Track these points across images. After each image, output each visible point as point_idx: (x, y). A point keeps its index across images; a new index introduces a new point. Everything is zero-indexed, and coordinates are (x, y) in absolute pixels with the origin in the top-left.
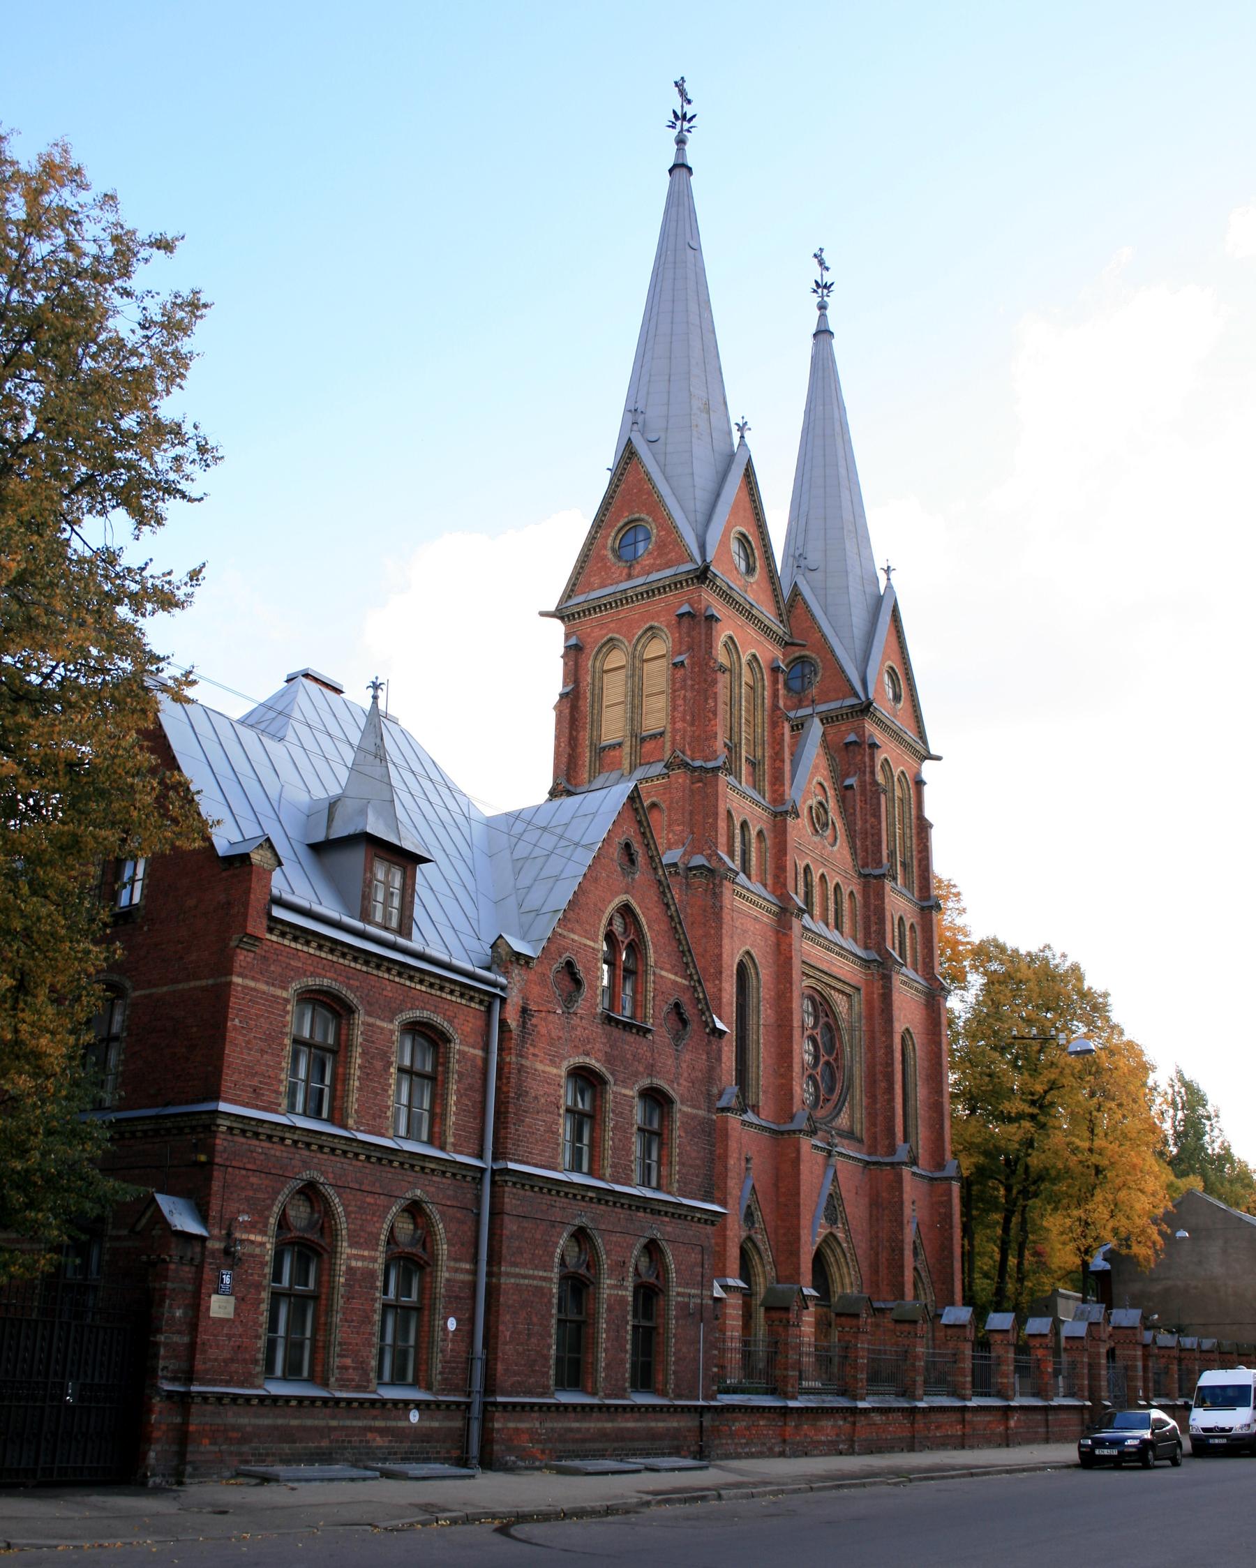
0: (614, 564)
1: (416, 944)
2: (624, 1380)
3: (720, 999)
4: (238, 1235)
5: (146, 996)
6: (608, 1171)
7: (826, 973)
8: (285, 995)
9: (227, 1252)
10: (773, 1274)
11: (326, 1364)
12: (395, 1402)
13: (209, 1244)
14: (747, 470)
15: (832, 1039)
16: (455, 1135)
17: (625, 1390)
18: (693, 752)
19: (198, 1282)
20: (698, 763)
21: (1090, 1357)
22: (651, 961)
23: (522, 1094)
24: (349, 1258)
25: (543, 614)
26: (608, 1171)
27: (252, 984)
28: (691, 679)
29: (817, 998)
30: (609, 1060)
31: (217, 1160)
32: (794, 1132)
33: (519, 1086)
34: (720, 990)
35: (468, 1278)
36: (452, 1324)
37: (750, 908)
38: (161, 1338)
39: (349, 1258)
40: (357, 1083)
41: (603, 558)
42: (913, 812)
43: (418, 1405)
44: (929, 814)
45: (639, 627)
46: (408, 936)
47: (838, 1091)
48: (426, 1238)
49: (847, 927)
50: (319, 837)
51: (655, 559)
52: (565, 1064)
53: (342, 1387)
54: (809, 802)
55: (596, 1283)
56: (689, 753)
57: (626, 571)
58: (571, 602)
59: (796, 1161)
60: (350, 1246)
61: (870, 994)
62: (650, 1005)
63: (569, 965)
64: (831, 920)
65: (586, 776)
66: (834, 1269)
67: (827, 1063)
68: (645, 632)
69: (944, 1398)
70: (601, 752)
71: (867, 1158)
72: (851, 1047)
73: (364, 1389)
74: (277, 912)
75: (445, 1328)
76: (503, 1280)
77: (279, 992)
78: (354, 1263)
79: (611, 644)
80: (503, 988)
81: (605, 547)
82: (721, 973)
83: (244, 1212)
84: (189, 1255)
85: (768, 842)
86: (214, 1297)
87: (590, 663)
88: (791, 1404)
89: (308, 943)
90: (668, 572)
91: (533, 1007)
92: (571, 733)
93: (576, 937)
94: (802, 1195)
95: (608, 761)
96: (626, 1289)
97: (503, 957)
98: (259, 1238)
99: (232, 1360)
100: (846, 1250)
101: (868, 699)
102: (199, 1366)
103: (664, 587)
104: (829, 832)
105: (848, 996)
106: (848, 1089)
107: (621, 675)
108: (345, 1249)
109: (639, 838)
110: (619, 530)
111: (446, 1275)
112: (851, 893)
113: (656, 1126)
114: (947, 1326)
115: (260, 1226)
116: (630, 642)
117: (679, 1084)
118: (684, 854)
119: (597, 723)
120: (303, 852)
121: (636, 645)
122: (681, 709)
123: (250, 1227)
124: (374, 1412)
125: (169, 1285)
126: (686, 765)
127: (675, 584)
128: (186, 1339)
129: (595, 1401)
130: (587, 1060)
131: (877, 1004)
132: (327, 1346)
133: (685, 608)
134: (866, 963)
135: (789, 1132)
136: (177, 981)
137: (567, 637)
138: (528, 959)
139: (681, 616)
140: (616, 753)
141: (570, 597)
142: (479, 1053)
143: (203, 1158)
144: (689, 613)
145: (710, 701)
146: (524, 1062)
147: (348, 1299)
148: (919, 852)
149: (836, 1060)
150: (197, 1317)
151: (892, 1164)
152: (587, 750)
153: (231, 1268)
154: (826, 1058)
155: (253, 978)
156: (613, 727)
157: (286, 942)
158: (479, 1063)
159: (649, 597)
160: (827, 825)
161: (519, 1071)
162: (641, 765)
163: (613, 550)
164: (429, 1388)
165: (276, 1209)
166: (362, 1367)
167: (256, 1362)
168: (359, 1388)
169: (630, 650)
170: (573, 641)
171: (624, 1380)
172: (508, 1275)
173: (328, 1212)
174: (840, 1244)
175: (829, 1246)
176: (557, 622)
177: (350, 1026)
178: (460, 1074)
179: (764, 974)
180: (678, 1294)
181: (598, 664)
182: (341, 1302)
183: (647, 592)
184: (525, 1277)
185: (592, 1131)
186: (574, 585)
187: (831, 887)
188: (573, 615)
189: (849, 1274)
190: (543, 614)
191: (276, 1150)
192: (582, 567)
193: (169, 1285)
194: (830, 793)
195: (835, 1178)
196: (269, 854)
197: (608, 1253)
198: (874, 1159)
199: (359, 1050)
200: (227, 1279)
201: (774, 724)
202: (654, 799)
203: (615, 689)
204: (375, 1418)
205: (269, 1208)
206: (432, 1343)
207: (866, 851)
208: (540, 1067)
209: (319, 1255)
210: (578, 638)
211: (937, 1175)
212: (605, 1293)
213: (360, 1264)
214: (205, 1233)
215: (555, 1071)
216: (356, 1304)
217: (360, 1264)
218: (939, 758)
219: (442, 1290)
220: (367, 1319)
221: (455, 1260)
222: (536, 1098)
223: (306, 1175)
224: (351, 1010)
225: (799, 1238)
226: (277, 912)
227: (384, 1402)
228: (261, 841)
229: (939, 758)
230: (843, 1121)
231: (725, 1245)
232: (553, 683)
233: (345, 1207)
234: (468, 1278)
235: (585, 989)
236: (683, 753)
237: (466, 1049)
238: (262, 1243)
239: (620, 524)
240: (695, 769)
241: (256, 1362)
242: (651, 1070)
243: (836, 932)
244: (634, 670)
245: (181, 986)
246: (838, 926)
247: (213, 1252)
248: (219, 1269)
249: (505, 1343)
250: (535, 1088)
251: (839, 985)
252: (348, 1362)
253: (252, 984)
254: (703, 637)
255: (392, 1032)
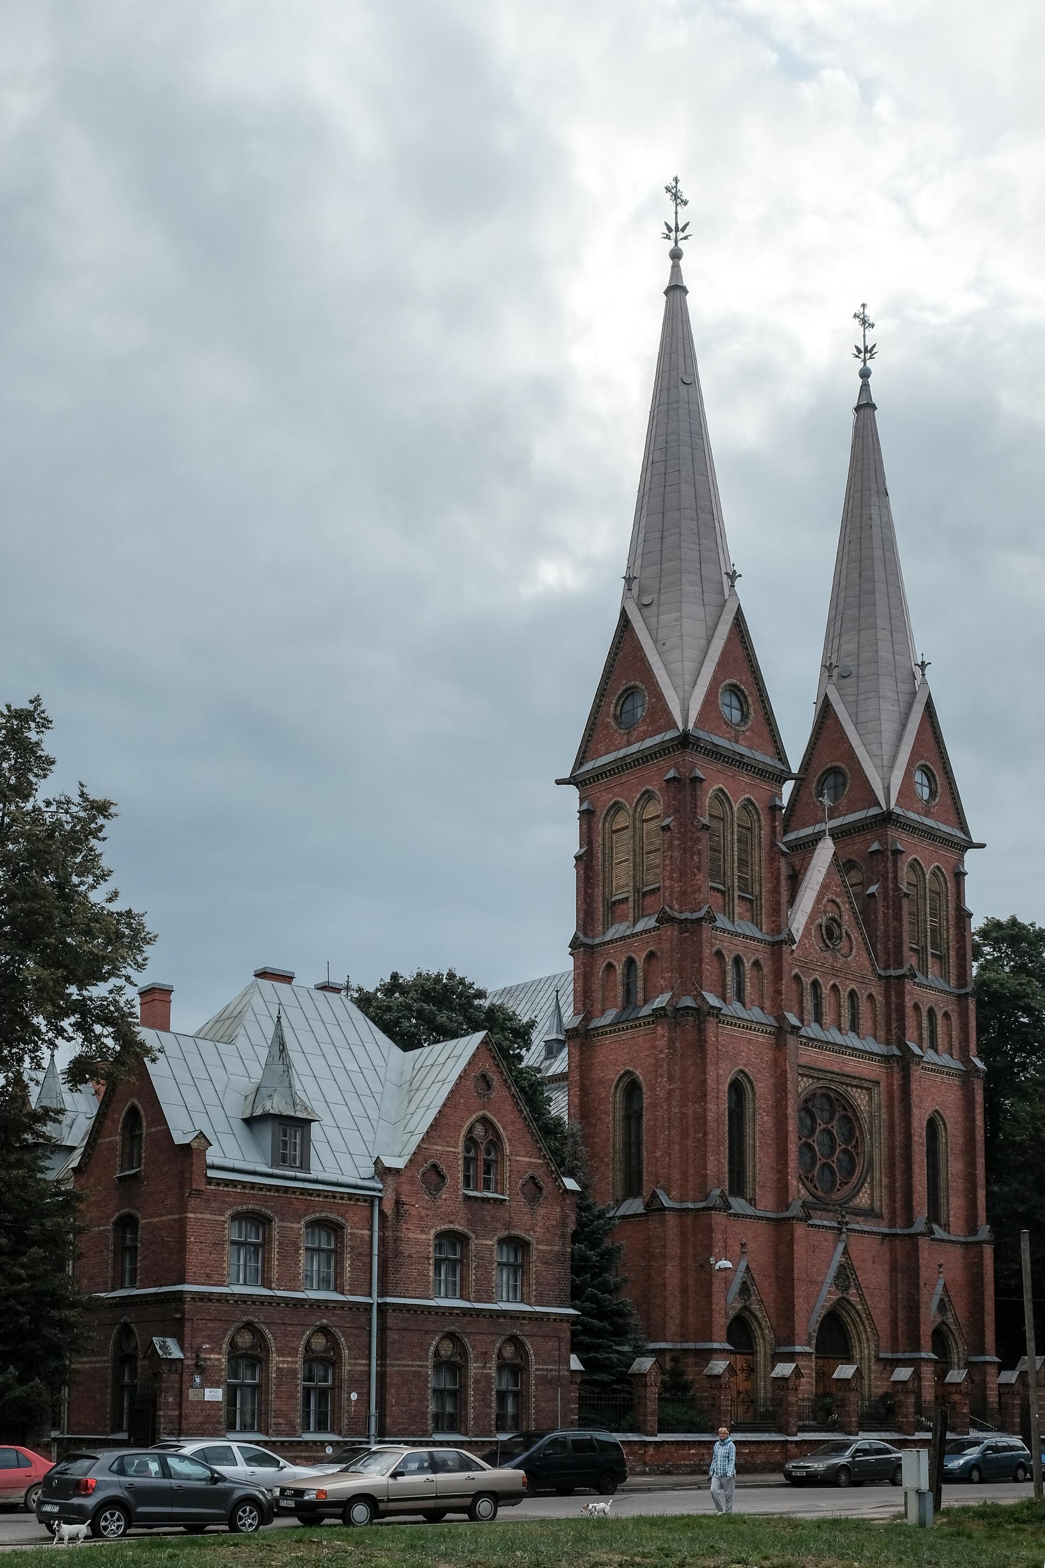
0: (616, 731)
1: (313, 1175)
2: (491, 1426)
3: (705, 1118)
4: (203, 1356)
5: (149, 1223)
6: (473, 1295)
7: (838, 1074)
8: (223, 1218)
9: (197, 1366)
10: (772, 1336)
11: (267, 1423)
12: (315, 1442)
13: (186, 1362)
14: (736, 619)
15: (851, 1130)
16: (350, 1285)
17: (491, 1431)
18: (681, 906)
19: (181, 1382)
20: (683, 916)
21: (1021, 1399)
22: (508, 1152)
23: (398, 1253)
24: (277, 1363)
25: (559, 782)
26: (473, 1295)
27: (200, 1216)
28: (679, 839)
29: (832, 1094)
30: (470, 1223)
31: (187, 1316)
32: (788, 1219)
33: (396, 1249)
34: (705, 1110)
35: (367, 1368)
36: (354, 1396)
37: (742, 1033)
38: (161, 1413)
39: (277, 1363)
40: (276, 1263)
41: (607, 726)
42: (952, 905)
43: (331, 1443)
44: (969, 904)
45: (638, 791)
46: (308, 1170)
47: (857, 1174)
48: (334, 1345)
49: (865, 1024)
50: (247, 1115)
51: (648, 725)
52: (433, 1232)
53: (278, 1435)
54: (819, 921)
55: (466, 1368)
56: (677, 907)
57: (626, 737)
58: (588, 766)
59: (791, 1243)
60: (279, 1356)
61: (890, 1085)
62: (507, 1182)
63: (434, 1166)
64: (846, 1023)
65: (600, 928)
66: (851, 1327)
67: (845, 1151)
68: (643, 795)
69: (894, 1433)
70: (612, 906)
71: (886, 1230)
72: (871, 1134)
73: (293, 1435)
74: (211, 1173)
75: (349, 1399)
76: (388, 1369)
77: (219, 1218)
78: (281, 1366)
79: (617, 807)
80: (380, 1191)
81: (608, 714)
82: (705, 1095)
83: (206, 1343)
84: (174, 1368)
85: (765, 970)
86: (191, 1390)
87: (600, 825)
88: (790, 1439)
89: (236, 1187)
90: (657, 739)
91: (403, 1198)
92: (586, 892)
93: (439, 1148)
94: (796, 1271)
95: (618, 913)
96: (490, 1368)
97: (382, 1172)
98: (217, 1356)
99: (205, 1422)
100: (861, 1312)
101: (888, 809)
102: (184, 1426)
103: (655, 753)
104: (844, 944)
105: (868, 1089)
106: (867, 1172)
107: (629, 832)
108: (275, 1358)
109: (494, 1069)
110: (616, 706)
111: (349, 1368)
112: (870, 996)
113: (519, 1261)
114: (837, 1380)
115: (217, 1350)
116: (630, 805)
117: (534, 1231)
118: (672, 997)
119: (607, 880)
120: (239, 1127)
121: (636, 808)
122: (668, 868)
123: (212, 1351)
124: (300, 1448)
125: (164, 1385)
126: (672, 919)
127: (664, 750)
128: (177, 1413)
129: (466, 1439)
130: (452, 1226)
131: (897, 1094)
132: (267, 1412)
133: (671, 774)
134: (887, 1058)
135: (784, 1219)
136: (161, 1215)
137: (582, 801)
138: (398, 1171)
139: (668, 781)
140: (624, 906)
141: (581, 764)
142: (367, 1232)
143: (178, 1316)
144: (674, 778)
145: (695, 857)
146: (398, 1234)
147: (278, 1386)
148: (957, 942)
149: (855, 1147)
150: (181, 1400)
151: (910, 1235)
152: (601, 905)
153: (200, 1374)
154: (843, 1146)
155: (201, 1213)
156: (621, 881)
157: (221, 1188)
158: (367, 1239)
159: (644, 763)
160: (841, 937)
161: (395, 1240)
162: (643, 916)
163: (615, 716)
164: (340, 1434)
165: (226, 1340)
166: (291, 1424)
167: (220, 1423)
168: (288, 1435)
169: (631, 813)
170: (585, 806)
171: (491, 1426)
172: (392, 1365)
173: (263, 1337)
174: (854, 1308)
175: (844, 1308)
176: (572, 788)
177: (270, 1229)
178: (353, 1248)
179: (762, 1088)
180: (537, 1370)
181: (607, 825)
182: (274, 1388)
183: (642, 758)
184: (406, 1366)
185: (462, 1269)
186: (585, 752)
187: (844, 995)
188: (585, 780)
189: (866, 1331)
190: (559, 782)
191: (225, 1307)
192: (590, 735)
193: (164, 1385)
194: (845, 907)
195: (846, 1252)
196: (203, 1141)
197: (473, 1348)
198: (893, 1231)
199: (277, 1243)
200: (198, 1380)
201: (772, 860)
202: (652, 948)
203: (623, 850)
204: (301, 1451)
205: (222, 1339)
206: (340, 1408)
207: (888, 954)
208: (411, 1235)
209: (261, 1363)
210: (591, 803)
211: (971, 1239)
212: (472, 1372)
213: (285, 1366)
214: (182, 1357)
215: (424, 1237)
216: (284, 1388)
217: (285, 1366)
218: (982, 846)
219: (345, 1376)
220: (292, 1396)
221: (356, 1359)
222: (410, 1256)
223: (245, 1319)
224: (270, 1220)
225: (793, 1306)
226: (211, 1173)
227: (307, 1442)
228: (197, 1133)
229: (982, 846)
230: (863, 1200)
231: (711, 1317)
232: (571, 842)
233: (273, 1334)
234: (367, 1368)
235: (448, 1181)
236: (671, 908)
237: (356, 1231)
238: (219, 1359)
239: (620, 692)
240: (681, 922)
241: (220, 1423)
242: (508, 1225)
243: (851, 1034)
244: (634, 831)
245: (164, 1218)
246: (854, 1027)
247: (188, 1367)
248: (192, 1375)
249: (392, 1406)
250: (407, 1249)
251: (855, 1082)
252: (281, 1420)
253: (200, 1216)
254: (688, 799)
255: (300, 1229)
